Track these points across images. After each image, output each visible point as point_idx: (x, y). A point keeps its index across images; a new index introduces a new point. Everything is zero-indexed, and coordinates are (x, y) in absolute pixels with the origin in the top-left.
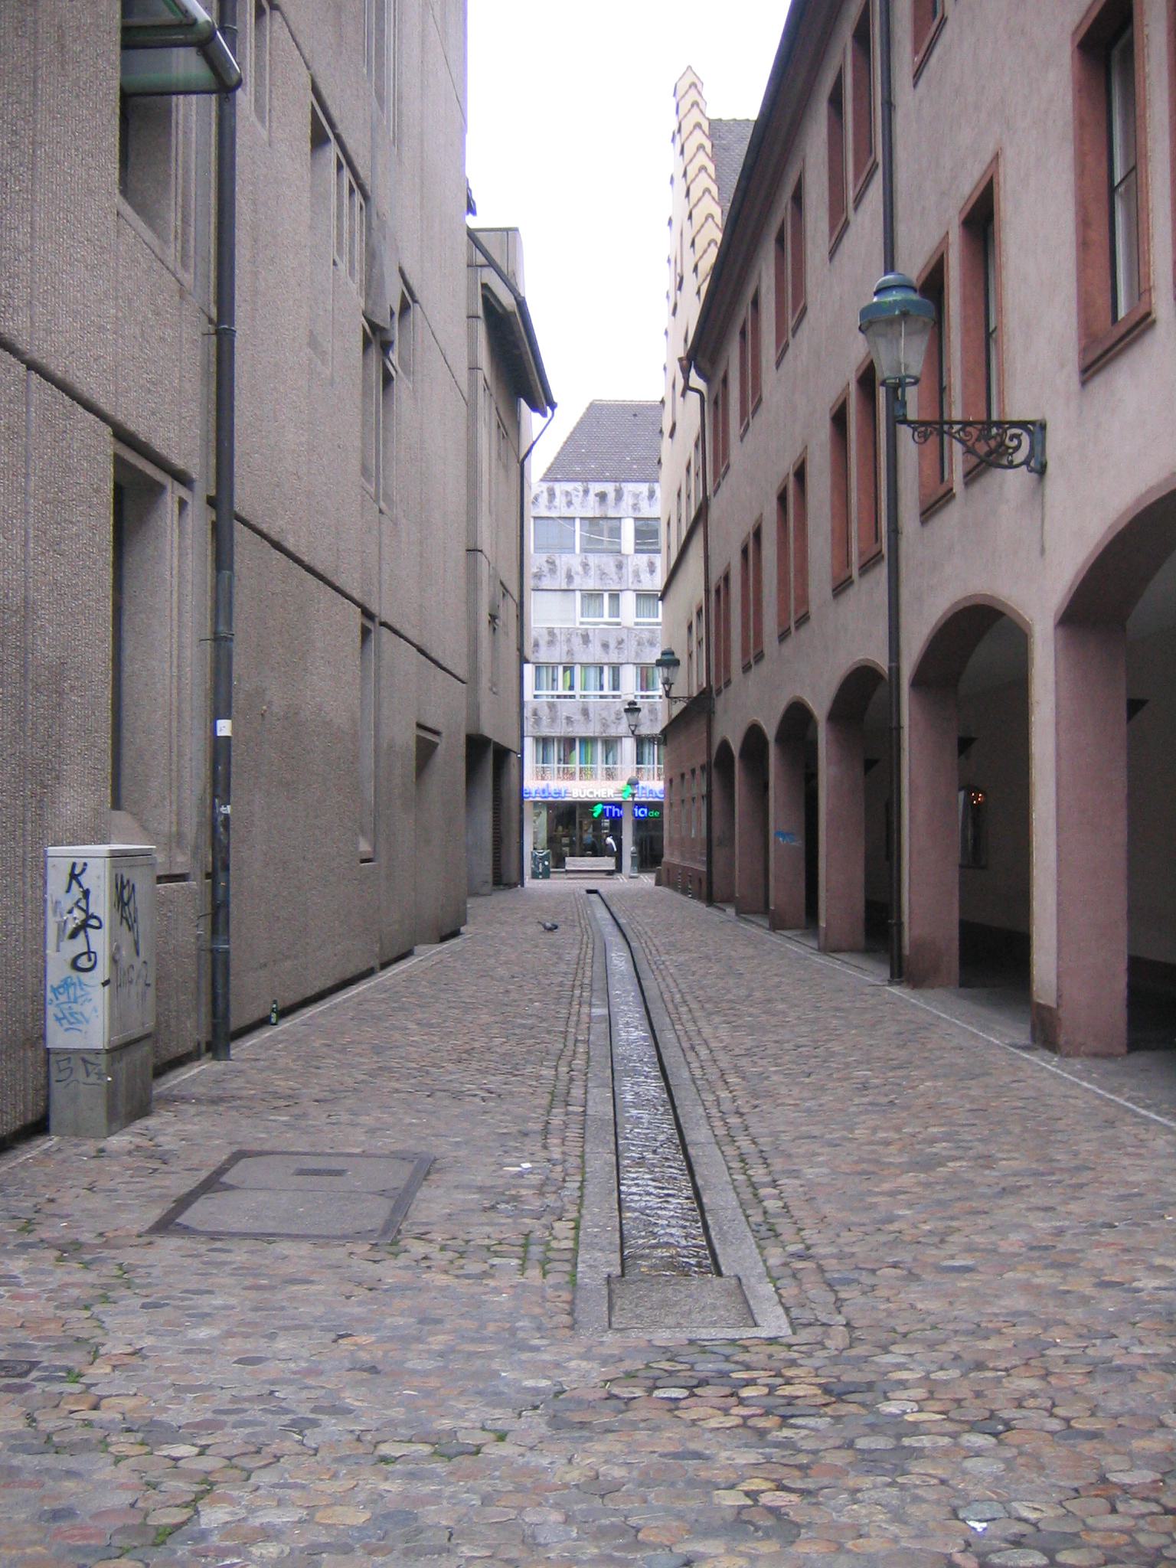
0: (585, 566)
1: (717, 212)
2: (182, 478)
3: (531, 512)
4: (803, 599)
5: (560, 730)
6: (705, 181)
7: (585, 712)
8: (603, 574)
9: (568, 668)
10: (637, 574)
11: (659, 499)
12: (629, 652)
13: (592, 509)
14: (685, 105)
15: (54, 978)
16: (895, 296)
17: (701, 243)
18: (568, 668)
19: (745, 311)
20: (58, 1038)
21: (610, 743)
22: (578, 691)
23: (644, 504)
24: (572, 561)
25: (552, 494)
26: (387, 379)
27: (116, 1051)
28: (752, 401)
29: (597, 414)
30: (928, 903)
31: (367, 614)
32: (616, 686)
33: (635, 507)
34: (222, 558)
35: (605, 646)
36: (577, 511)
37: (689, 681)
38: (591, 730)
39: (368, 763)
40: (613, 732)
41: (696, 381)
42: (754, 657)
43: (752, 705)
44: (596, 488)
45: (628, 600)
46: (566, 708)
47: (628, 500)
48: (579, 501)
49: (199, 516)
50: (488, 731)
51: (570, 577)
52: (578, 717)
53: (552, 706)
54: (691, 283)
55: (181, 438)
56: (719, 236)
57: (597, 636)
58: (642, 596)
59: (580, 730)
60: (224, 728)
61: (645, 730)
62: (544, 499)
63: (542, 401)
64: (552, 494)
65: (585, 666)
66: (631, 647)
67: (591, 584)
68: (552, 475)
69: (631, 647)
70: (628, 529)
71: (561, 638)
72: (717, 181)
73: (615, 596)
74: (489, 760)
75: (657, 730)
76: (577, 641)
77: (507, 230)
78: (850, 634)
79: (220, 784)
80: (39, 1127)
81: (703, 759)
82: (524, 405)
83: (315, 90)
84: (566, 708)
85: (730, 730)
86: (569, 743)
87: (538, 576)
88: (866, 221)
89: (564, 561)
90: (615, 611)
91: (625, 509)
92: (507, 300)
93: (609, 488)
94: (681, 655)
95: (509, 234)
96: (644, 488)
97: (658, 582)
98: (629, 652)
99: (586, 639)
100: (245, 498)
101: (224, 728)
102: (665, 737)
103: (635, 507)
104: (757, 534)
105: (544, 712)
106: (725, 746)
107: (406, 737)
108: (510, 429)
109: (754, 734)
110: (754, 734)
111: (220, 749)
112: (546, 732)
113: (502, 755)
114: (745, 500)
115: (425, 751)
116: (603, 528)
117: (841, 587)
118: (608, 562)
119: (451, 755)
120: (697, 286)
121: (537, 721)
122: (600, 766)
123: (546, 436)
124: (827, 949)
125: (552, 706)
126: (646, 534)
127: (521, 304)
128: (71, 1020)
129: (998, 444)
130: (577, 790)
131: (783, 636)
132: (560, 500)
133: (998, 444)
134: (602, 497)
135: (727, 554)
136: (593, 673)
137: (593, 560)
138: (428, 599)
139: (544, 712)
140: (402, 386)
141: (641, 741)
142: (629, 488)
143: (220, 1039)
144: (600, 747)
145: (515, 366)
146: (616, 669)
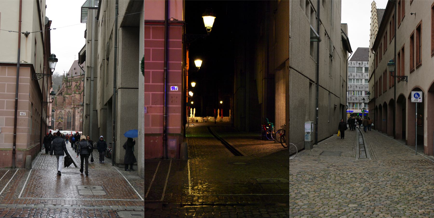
0: (357, 75)
1: (377, 25)
2: (314, 82)
3: (348, 66)
4: (386, 89)
5: (352, 101)
6: (376, 21)
7: (356, 99)
8: (359, 76)
9: (354, 91)
10: (365, 76)
11: (368, 64)
12: (364, 89)
13: (358, 66)
14: (373, 7)
15: (305, 135)
16: (391, 62)
17: (375, 30)
18: (354, 91)
19: (380, 45)
20: (306, 140)
21: (360, 104)
22: (355, 95)
23: (366, 65)
24: (354, 74)
25: (351, 63)
26: (332, 60)
27: (311, 141)
28: (381, 59)
29: (359, 49)
30: (398, 130)
31: (329, 92)
32: (361, 94)
33: (365, 65)
34: (317, 90)
35: (360, 88)
36: (355, 66)
37: (372, 97)
38: (357, 101)
39: (329, 111)
40: (361, 102)
41: (374, 52)
42: (380, 95)
43: (380, 101)
44: (358, 62)
45: (363, 80)
46: (353, 98)
47: (364, 64)
48: (356, 64)
49: (315, 85)
50: (342, 103)
51: (354, 77)
52: (355, 99)
53: (351, 98)
54: (373, 36)
55: (314, 79)
56: (378, 30)
57: (359, 84)
58: (366, 80)
59: (355, 101)
60: (317, 109)
61: (366, 102)
62: (350, 64)
63: (351, 51)
64: (351, 63)
65: (356, 91)
66: (364, 88)
67: (358, 78)
68: (351, 60)
69: (364, 88)
70: (364, 69)
71: (352, 86)
72: (378, 24)
73: (361, 80)
74: (343, 107)
75: (368, 102)
76: (355, 87)
77: (345, 24)
78: (389, 96)
79: (317, 115)
80: (304, 149)
81: (374, 108)
82: (347, 52)
83: (325, 30)
84: (353, 98)
85: (377, 104)
86: (354, 103)
87: (349, 76)
88: (393, 41)
89: (353, 74)
90: (361, 82)
91: (363, 66)
92: (345, 38)
93: (361, 62)
94: (371, 92)
95: (345, 25)
96: (366, 62)
97: (368, 78)
98: (364, 89)
99: (356, 87)
100: (320, 83)
101: (317, 109)
102: (369, 104)
103: (365, 65)
104: (381, 77)
105: (350, 99)
106: (377, 106)
107: (333, 107)
108: (345, 56)
109: (380, 105)
110: (380, 105)
111: (317, 111)
112: (350, 102)
113: (343, 106)
114: (380, 72)
115: (335, 108)
116: (360, 68)
117: (390, 88)
118: (360, 74)
119: (338, 107)
120: (374, 37)
121: (348, 100)
122: (358, 107)
123: (350, 56)
124: (388, 135)
125: (351, 98)
126: (366, 69)
127: (348, 39)
128: (307, 139)
129: (403, 78)
130: (355, 111)
131: (384, 93)
132: (353, 64)
133: (403, 78)
134: (360, 64)
135: (377, 79)
136: (358, 92)
137: (358, 74)
138: (336, 88)
139: (350, 99)
140: (333, 61)
141: (365, 104)
142: (364, 62)
143: (316, 143)
144: (358, 104)
145: (346, 45)
146: (361, 92)
